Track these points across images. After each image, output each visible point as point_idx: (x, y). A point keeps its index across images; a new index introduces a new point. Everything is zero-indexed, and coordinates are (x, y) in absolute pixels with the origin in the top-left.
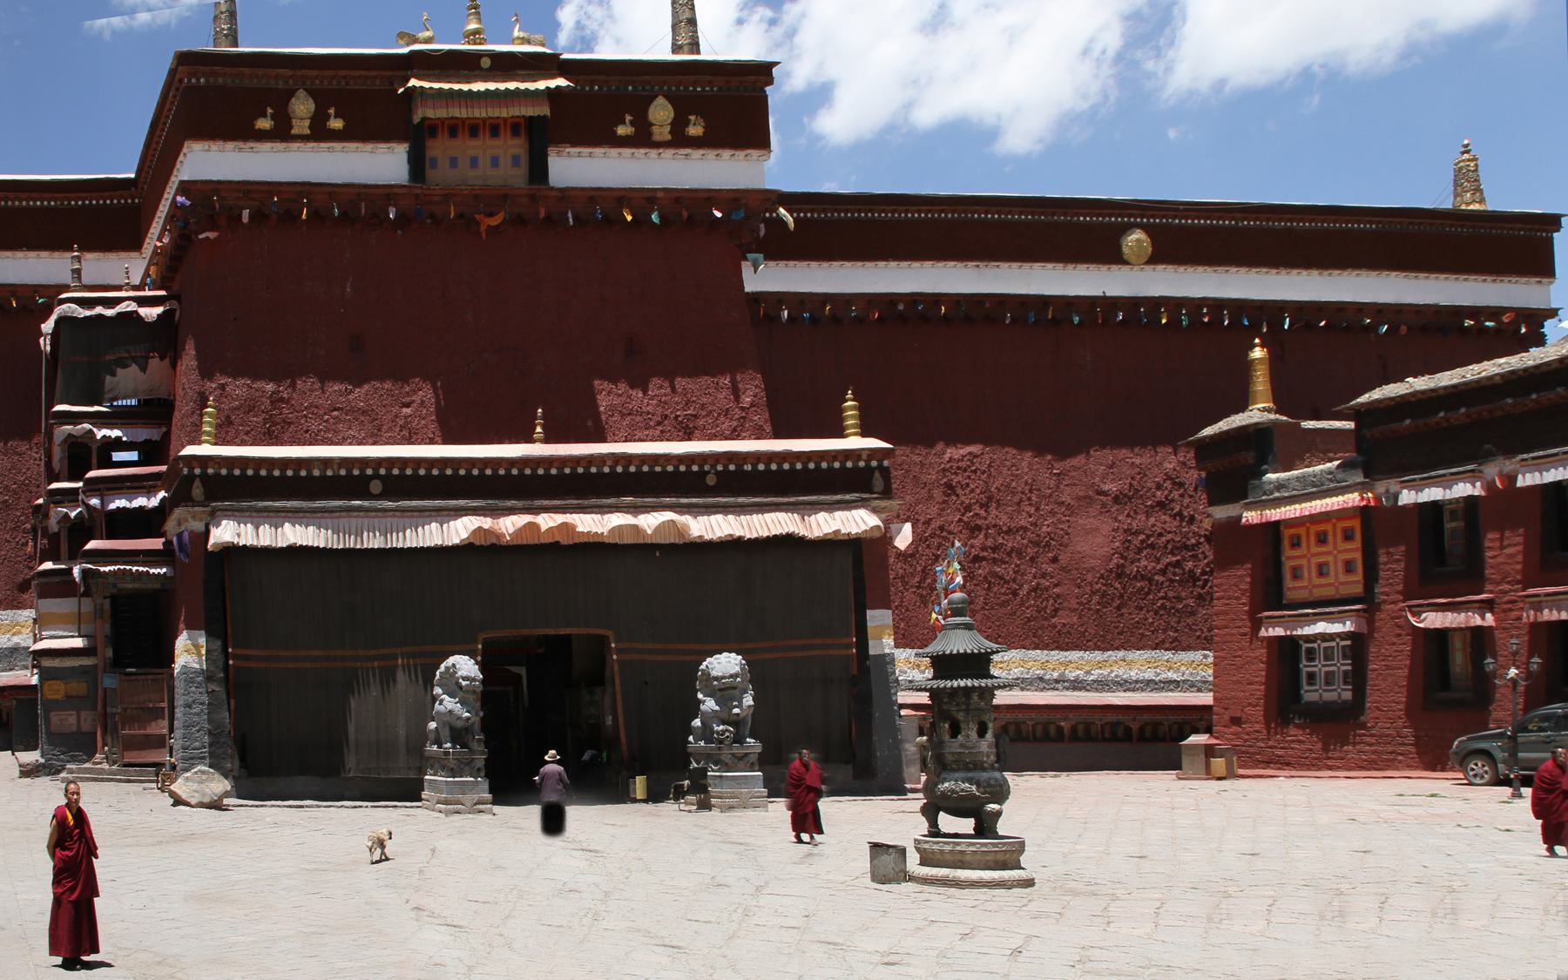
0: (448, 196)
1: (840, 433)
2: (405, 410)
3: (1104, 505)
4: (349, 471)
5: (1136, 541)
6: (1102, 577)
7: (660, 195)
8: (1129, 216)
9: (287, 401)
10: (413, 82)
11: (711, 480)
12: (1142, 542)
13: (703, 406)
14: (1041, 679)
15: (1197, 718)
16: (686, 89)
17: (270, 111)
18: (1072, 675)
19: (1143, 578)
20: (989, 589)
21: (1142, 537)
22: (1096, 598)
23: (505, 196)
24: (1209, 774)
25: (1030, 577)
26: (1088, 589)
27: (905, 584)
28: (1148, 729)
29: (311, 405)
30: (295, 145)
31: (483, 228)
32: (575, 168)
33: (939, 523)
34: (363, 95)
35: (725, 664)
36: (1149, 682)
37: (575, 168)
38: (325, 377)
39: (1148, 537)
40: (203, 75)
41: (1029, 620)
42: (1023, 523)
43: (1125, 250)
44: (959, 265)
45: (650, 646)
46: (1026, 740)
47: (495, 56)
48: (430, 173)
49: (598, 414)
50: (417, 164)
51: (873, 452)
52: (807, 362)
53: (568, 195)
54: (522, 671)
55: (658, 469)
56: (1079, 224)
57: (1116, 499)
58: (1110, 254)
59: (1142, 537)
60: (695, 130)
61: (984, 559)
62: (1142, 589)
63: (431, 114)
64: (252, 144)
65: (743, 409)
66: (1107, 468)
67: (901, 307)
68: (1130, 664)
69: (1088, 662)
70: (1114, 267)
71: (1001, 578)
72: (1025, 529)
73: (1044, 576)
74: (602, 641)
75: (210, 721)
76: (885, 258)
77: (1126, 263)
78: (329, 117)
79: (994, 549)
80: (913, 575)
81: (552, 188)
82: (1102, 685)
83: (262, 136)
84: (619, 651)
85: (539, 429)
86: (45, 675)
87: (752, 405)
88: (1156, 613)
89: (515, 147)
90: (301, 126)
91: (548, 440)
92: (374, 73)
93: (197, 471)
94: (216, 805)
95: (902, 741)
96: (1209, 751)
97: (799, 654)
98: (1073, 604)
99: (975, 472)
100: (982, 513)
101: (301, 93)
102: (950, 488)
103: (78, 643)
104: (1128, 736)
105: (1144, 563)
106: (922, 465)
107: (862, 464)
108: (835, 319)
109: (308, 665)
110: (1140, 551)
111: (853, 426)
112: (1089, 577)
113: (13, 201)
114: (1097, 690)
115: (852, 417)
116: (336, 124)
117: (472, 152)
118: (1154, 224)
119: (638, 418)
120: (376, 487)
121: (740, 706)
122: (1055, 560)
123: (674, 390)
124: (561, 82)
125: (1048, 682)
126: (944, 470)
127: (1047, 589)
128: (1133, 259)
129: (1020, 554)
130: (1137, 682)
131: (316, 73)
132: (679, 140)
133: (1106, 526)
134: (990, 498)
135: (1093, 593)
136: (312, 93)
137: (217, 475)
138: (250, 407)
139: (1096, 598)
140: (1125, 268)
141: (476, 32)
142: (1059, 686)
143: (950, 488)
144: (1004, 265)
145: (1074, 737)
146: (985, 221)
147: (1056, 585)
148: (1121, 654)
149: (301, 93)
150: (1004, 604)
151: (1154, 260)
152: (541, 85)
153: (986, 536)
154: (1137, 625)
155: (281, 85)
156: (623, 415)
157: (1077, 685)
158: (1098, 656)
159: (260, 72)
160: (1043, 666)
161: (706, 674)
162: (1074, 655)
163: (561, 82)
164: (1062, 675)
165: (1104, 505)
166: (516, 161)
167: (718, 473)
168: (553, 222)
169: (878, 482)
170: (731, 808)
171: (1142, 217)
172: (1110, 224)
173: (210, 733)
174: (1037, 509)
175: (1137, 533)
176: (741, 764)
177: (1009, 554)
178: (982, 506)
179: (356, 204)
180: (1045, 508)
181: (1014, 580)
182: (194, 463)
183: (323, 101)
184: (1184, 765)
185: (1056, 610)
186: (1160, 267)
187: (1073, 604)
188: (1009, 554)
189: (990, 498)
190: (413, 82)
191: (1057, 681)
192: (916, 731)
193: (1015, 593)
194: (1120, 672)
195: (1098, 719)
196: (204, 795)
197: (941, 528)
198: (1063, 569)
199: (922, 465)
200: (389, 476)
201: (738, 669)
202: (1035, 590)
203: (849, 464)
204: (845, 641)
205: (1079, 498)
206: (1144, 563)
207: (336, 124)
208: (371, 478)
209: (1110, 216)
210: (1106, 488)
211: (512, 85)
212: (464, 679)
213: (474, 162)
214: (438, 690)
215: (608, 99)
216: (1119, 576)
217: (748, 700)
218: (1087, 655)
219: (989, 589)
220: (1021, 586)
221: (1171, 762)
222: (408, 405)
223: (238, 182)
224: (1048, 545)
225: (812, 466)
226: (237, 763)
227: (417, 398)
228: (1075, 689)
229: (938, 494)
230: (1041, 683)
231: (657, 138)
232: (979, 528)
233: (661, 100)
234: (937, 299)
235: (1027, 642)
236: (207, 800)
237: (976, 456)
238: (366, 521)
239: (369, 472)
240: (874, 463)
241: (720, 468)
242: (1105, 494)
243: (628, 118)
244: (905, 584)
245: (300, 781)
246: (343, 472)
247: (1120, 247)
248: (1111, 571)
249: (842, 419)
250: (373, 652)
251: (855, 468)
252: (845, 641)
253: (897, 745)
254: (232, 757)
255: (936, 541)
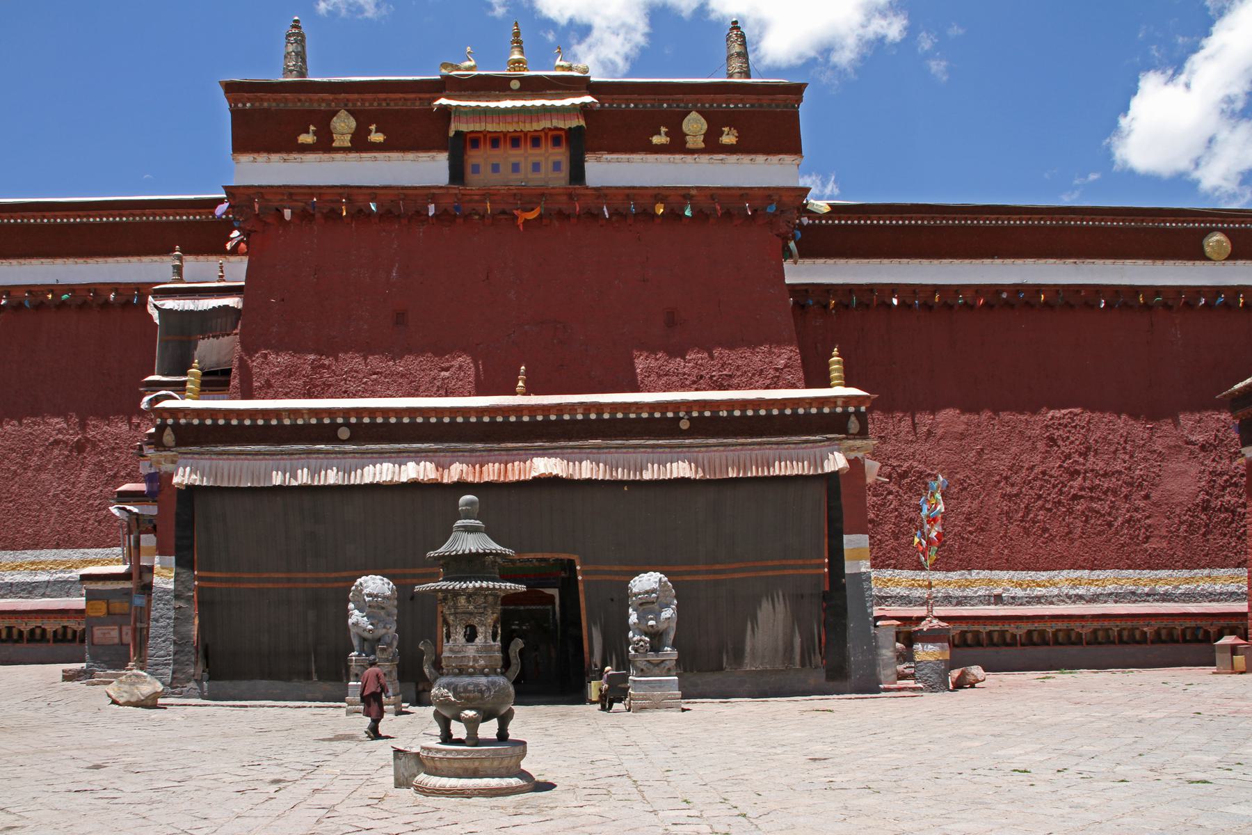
0: (487, 194)
1: (827, 384)
2: (443, 373)
3: (1191, 453)
4: (320, 420)
5: (1221, 481)
6: (1189, 510)
7: (693, 192)
8: (1211, 222)
9: (329, 367)
10: (443, 101)
11: (684, 425)
12: (1226, 481)
13: (738, 368)
14: (1133, 593)
15: (1233, 623)
16: (719, 106)
17: (312, 128)
18: (1161, 589)
19: (1227, 510)
20: (1086, 521)
21: (1225, 477)
22: (1184, 527)
23: (543, 194)
24: (1234, 671)
25: (1124, 511)
26: (1176, 520)
27: (1009, 518)
28: (1125, 633)
29: (351, 370)
30: (338, 156)
31: (520, 221)
32: (607, 170)
33: (1041, 469)
34: (402, 116)
35: (646, 582)
36: (1232, 594)
37: (607, 170)
38: (367, 350)
39: (1231, 477)
40: (249, 100)
41: (1123, 546)
42: (1118, 468)
43: (1207, 249)
44: (1058, 261)
45: (616, 568)
46: (1113, 643)
47: (523, 80)
48: (471, 177)
49: (635, 375)
50: (457, 172)
51: (848, 400)
52: (821, 325)
53: (602, 193)
54: (555, 592)
55: (632, 416)
56: (1165, 230)
57: (1203, 448)
58: (1196, 253)
59: (1225, 477)
60: (729, 138)
61: (1082, 497)
62: (1226, 519)
63: (464, 128)
64: (295, 156)
65: (776, 370)
66: (1199, 427)
67: (1004, 296)
68: (1214, 580)
69: (1176, 579)
70: (1198, 263)
71: (1098, 512)
72: (1120, 472)
73: (1136, 510)
74: (571, 564)
75: (175, 633)
76: (992, 257)
77: (1209, 259)
78: (370, 131)
79: (1091, 489)
80: (1017, 511)
81: (587, 188)
82: (1189, 597)
83: (305, 149)
84: (584, 573)
85: (520, 384)
86: (91, 596)
87: (786, 366)
88: (1239, 538)
89: (561, 154)
90: (342, 140)
91: (527, 393)
92: (412, 96)
93: (170, 421)
94: (149, 703)
95: (877, 647)
96: (1234, 650)
97: (770, 573)
98: (1164, 532)
99: (1075, 427)
100: (1081, 460)
101: (343, 113)
102: (1052, 441)
103: (121, 569)
104: (1171, 639)
105: (1227, 498)
106: (1027, 422)
107: (839, 410)
108: (948, 307)
109: (270, 586)
110: (1224, 488)
111: (837, 378)
112: (1178, 510)
113: (161, 216)
114: (1184, 601)
115: (836, 370)
116: (377, 137)
117: (514, 160)
118: (1234, 229)
119: (674, 378)
120: (344, 433)
121: (657, 618)
122: (1147, 497)
123: (711, 357)
124: (588, 99)
125: (1140, 595)
126: (1047, 426)
127: (1139, 520)
128: (1214, 256)
129: (1115, 493)
130: (1221, 594)
131: (356, 96)
132: (712, 146)
133: (1194, 468)
134: (1088, 449)
135: (1182, 523)
136: (352, 113)
137: (189, 425)
138: (291, 372)
139: (1184, 527)
140: (1207, 263)
141: (519, 61)
142: (1150, 599)
143: (1052, 441)
144: (1099, 262)
145: (1158, 639)
146: (1081, 227)
147: (1148, 517)
148: (1206, 571)
149: (343, 113)
150: (1100, 533)
151: (1233, 256)
152: (567, 102)
153: (1084, 479)
154: (1221, 548)
155: (323, 107)
156: (659, 376)
157: (1166, 597)
158: (1185, 573)
159: (303, 97)
160: (1136, 582)
161: (359, 591)
162: (1163, 573)
163: (588, 99)
164: (1153, 589)
165: (1191, 453)
166: (557, 166)
167: (691, 419)
168: (593, 216)
169: (854, 425)
170: (643, 709)
171: (1222, 223)
172: (1194, 229)
173: (175, 643)
174: (1132, 457)
175: (1221, 474)
176: (656, 670)
177: (1105, 493)
178: (1080, 455)
179: (401, 206)
180: (1138, 455)
181: (1109, 514)
182: (165, 415)
183: (364, 119)
184: (1217, 662)
185: (1148, 538)
186: (1240, 263)
187: (1164, 532)
188: (1105, 493)
189: (1088, 449)
190: (443, 101)
191: (1148, 595)
192: (893, 638)
193: (1110, 525)
194: (1206, 586)
195: (1179, 626)
196: (132, 695)
197: (1044, 473)
198: (1154, 504)
199: (1027, 422)
200: (360, 424)
201: (656, 586)
202: (1128, 521)
203: (826, 410)
204: (818, 561)
205: (1169, 448)
206: (1227, 498)
207: (377, 137)
208: (341, 425)
209: (1194, 222)
210: (1194, 439)
211: (538, 103)
212: (369, 595)
213: (516, 168)
214: (351, 606)
215: (629, 114)
216: (1204, 509)
217: (668, 613)
218: (1175, 573)
219: (1086, 521)
220: (1116, 519)
221: (1208, 660)
222: (447, 370)
223: (280, 187)
224: (1140, 485)
225: (788, 412)
226: (201, 667)
227: (456, 363)
228: (1164, 601)
229: (1041, 446)
230: (1133, 596)
231: (690, 145)
232: (1077, 472)
233: (694, 115)
234: (1038, 289)
235: (1121, 564)
236: (133, 699)
237: (1076, 415)
238: (325, 462)
239: (340, 420)
240: (851, 409)
241: (695, 414)
242: (1193, 443)
243: (663, 129)
244: (1009, 518)
245: (263, 684)
246: (314, 421)
247: (1202, 247)
248: (1197, 505)
249: (828, 373)
250: (334, 575)
251: (833, 414)
252: (818, 561)
253: (874, 650)
254: (196, 663)
255: (1038, 483)
